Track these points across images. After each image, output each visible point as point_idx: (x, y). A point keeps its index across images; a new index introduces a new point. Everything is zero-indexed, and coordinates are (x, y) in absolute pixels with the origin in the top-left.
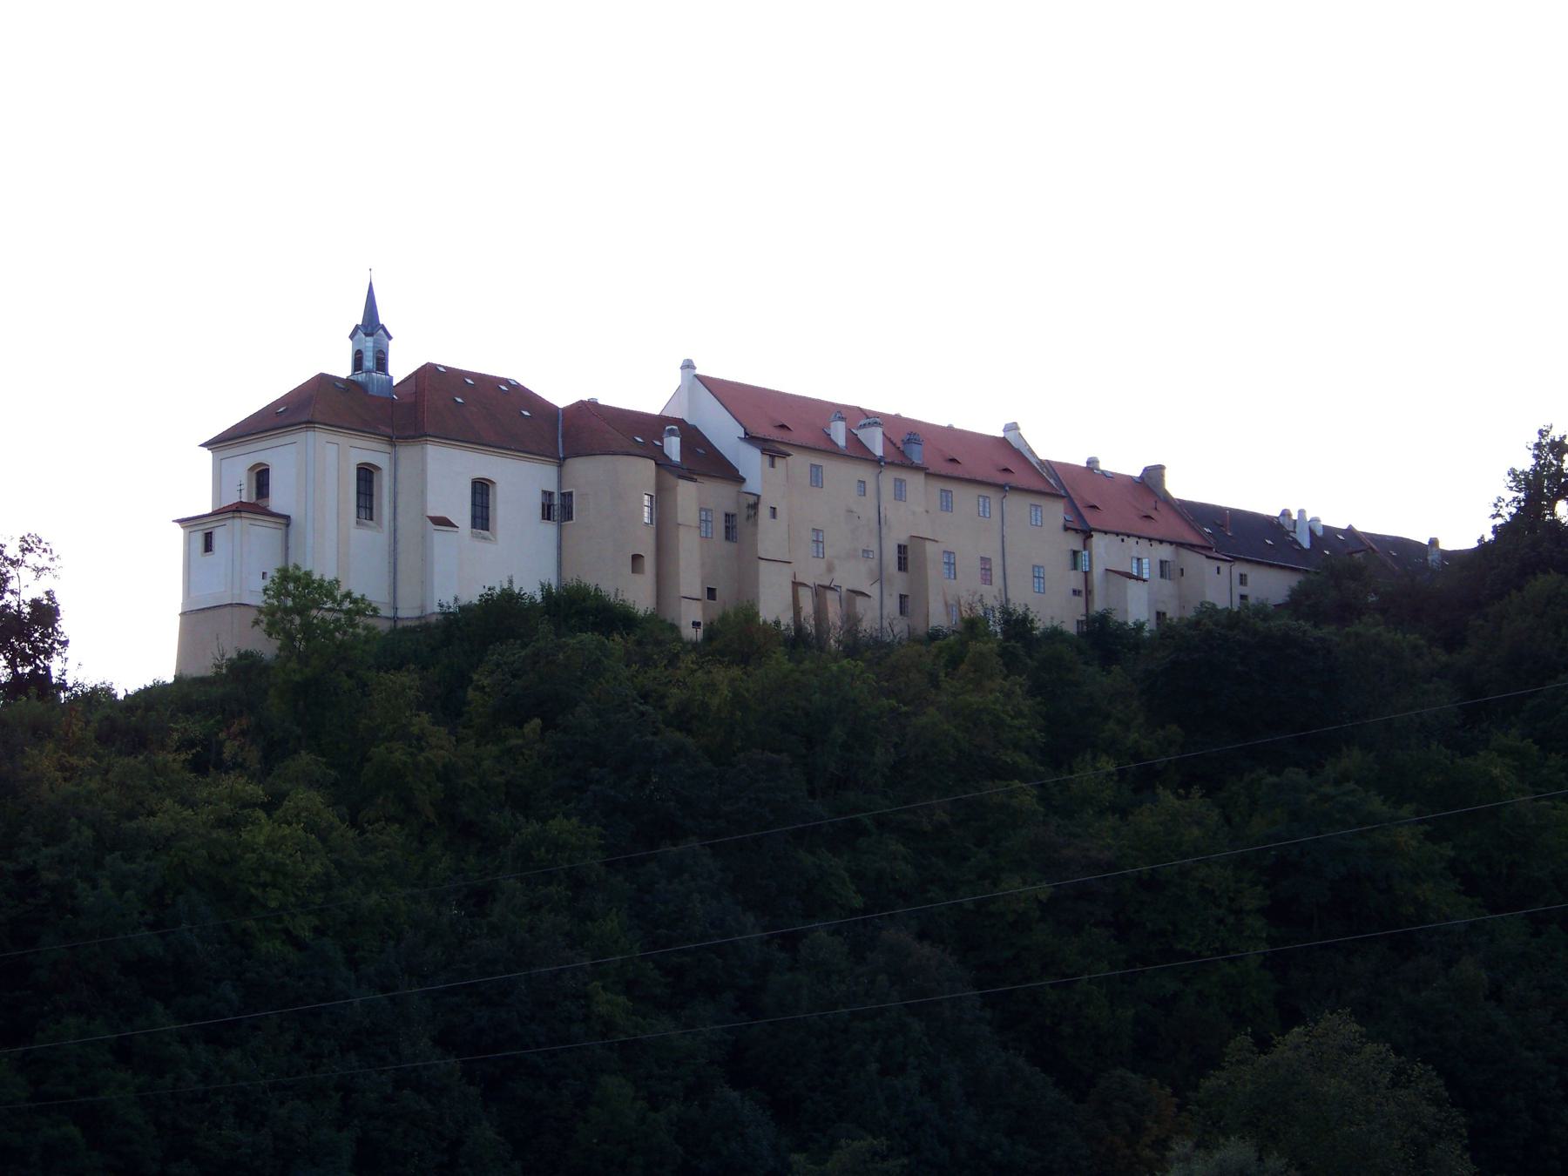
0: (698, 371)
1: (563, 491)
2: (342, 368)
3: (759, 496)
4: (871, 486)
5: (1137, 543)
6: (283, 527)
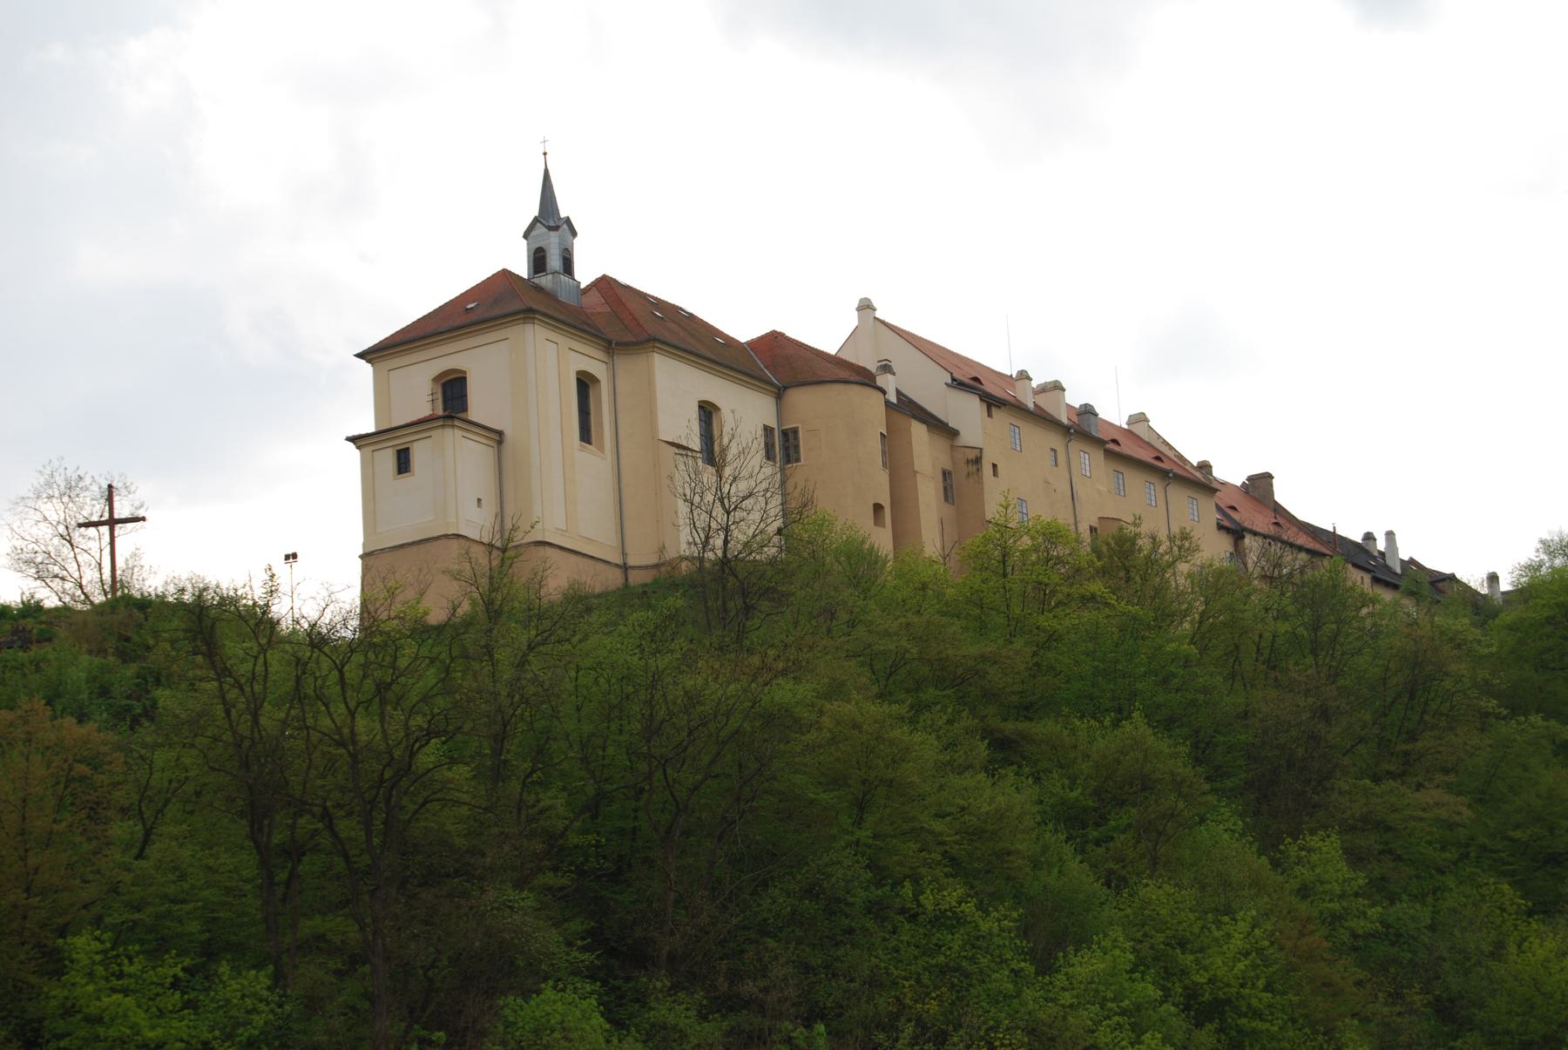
0: (878, 315)
1: (784, 428)
2: (520, 266)
3: (981, 449)
6: (495, 444)
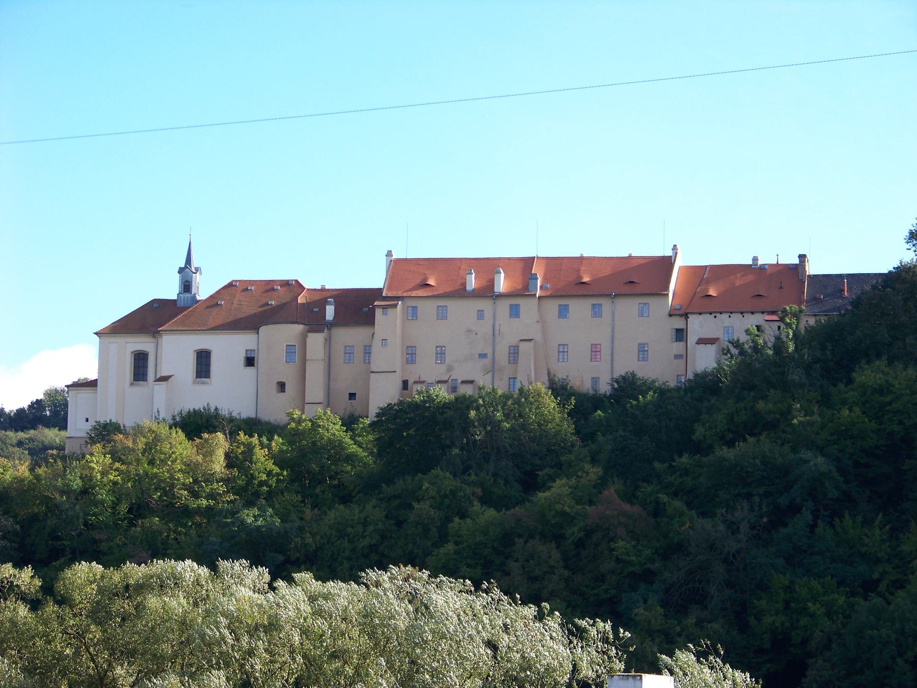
4: (488, 315)
5: (730, 316)
